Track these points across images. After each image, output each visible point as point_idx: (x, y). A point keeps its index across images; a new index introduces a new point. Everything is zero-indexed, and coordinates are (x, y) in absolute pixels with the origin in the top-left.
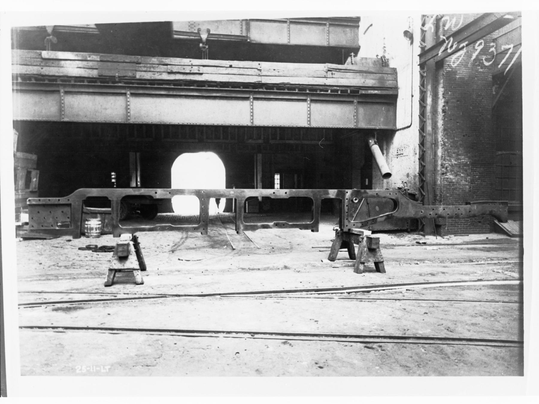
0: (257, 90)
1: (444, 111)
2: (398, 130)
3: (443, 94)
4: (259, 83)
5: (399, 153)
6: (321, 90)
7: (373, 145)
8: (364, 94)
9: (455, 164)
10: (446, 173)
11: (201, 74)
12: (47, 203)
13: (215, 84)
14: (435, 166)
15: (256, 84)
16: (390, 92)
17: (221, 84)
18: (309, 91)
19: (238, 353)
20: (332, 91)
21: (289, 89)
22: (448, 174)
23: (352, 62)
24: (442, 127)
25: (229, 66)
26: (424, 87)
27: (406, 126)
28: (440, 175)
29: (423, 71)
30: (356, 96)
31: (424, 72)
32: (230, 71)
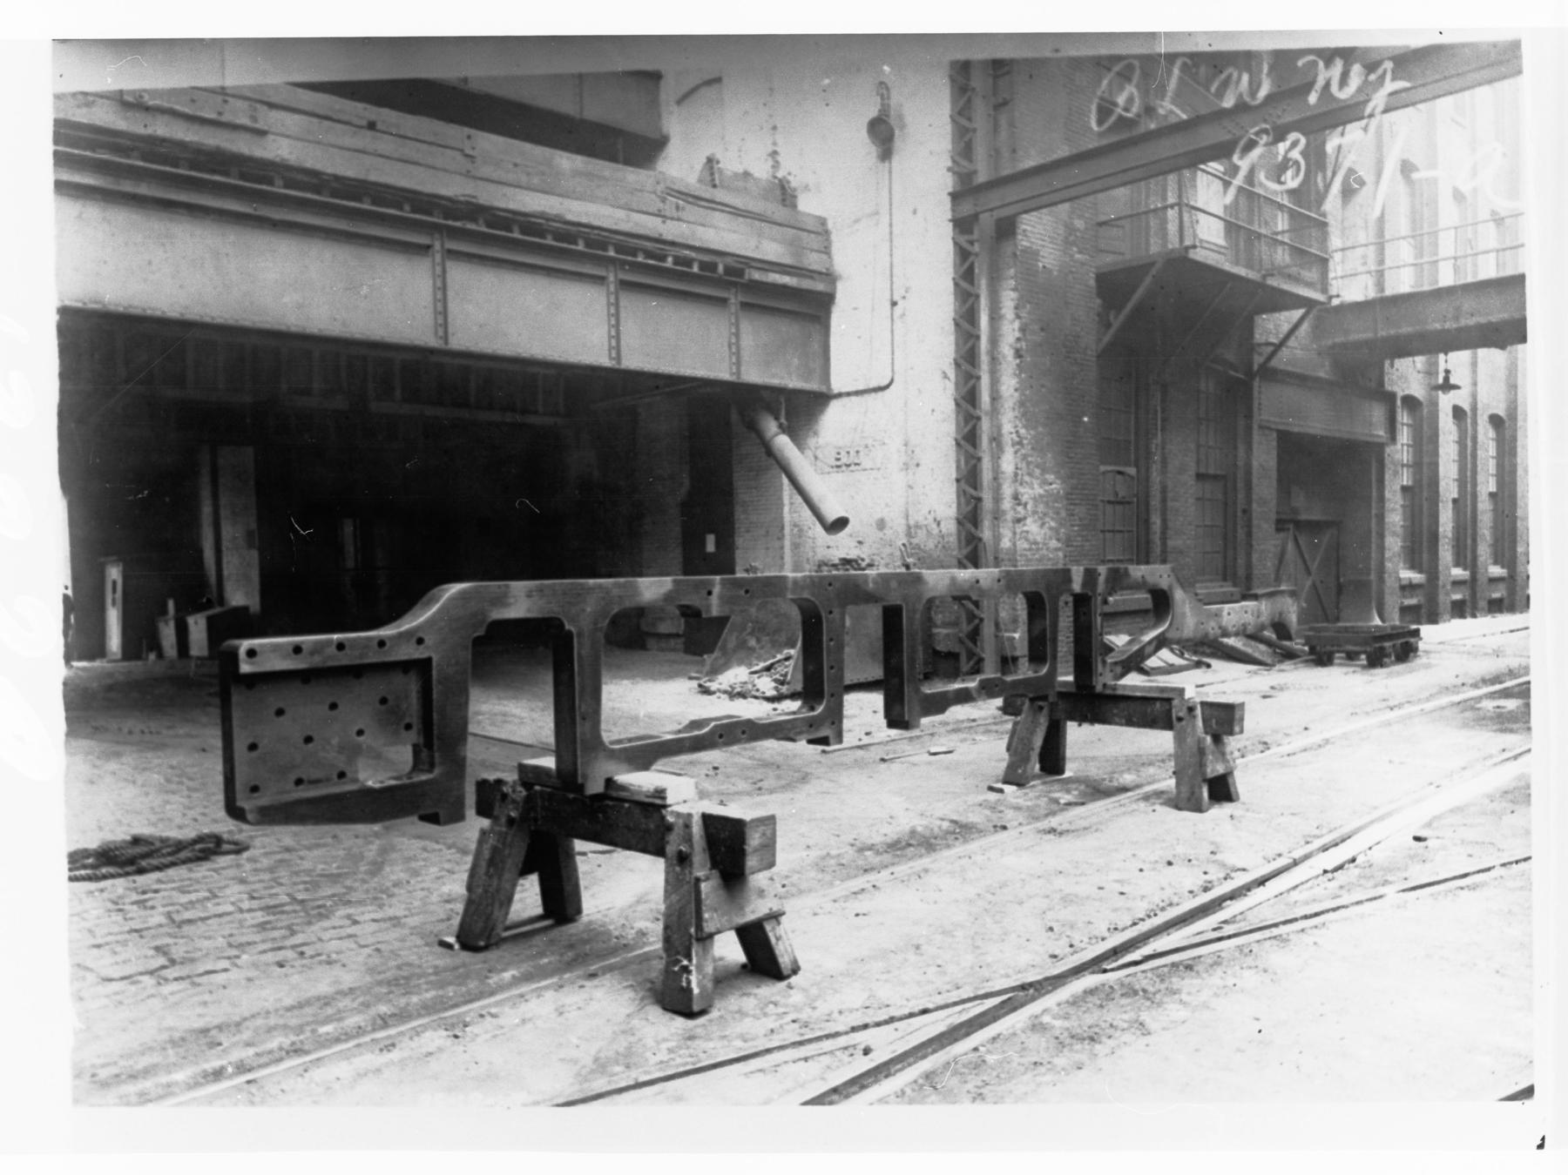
0: (458, 224)
1: (1018, 354)
2: (840, 395)
3: (1016, 308)
4: (468, 203)
5: (844, 460)
6: (649, 254)
7: (776, 435)
8: (757, 282)
9: (1041, 496)
10: (1025, 518)
11: (262, 133)
12: (330, 663)
13: (315, 181)
14: (997, 499)
15: (461, 202)
16: (820, 286)
17: (335, 185)
18: (617, 252)
19: (1541, 1146)
20: (677, 261)
21: (559, 236)
22: (1029, 521)
23: (713, 180)
24: (1016, 394)
25: (364, 123)
26: (972, 282)
27: (873, 384)
28: (1011, 525)
29: (967, 237)
30: (735, 284)
31: (971, 243)
32: (365, 140)
